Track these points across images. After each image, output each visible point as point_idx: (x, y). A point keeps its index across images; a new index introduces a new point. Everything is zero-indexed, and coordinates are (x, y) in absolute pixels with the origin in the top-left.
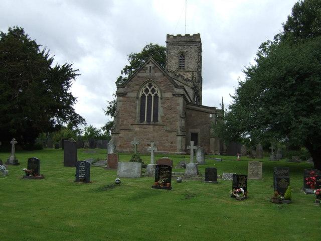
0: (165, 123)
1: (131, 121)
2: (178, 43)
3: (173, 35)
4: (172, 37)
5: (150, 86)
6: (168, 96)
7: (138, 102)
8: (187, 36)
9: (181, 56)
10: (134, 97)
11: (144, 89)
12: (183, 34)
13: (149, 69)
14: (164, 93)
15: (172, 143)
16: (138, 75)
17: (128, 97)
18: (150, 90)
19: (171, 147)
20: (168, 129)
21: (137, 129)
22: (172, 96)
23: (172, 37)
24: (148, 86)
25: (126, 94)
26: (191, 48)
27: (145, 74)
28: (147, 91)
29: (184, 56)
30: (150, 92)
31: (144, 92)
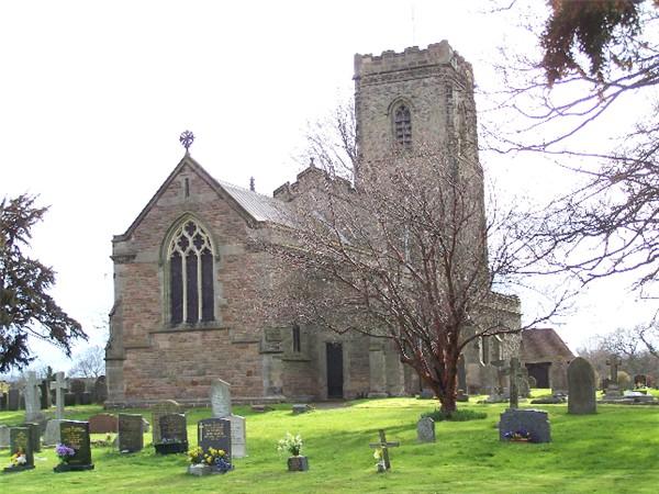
0: (230, 324)
1: (148, 325)
2: (387, 76)
3: (370, 56)
4: (369, 60)
5: (191, 228)
6: (235, 253)
7: (163, 275)
8: (412, 50)
9: (399, 114)
10: (154, 263)
11: (176, 239)
12: (399, 50)
13: (184, 185)
14: (224, 242)
15: (249, 374)
16: (158, 204)
17: (138, 264)
18: (190, 239)
19: (249, 384)
20: (238, 337)
21: (163, 342)
22: (242, 251)
23: (369, 60)
24: (187, 229)
25: (134, 257)
26: (425, 85)
27: (175, 201)
28: (184, 243)
29: (408, 113)
30: (191, 246)
31: (177, 247)
